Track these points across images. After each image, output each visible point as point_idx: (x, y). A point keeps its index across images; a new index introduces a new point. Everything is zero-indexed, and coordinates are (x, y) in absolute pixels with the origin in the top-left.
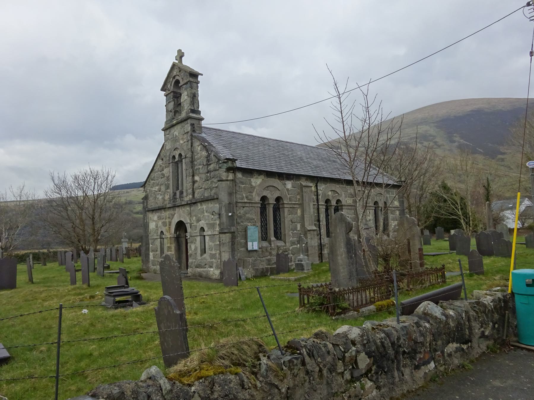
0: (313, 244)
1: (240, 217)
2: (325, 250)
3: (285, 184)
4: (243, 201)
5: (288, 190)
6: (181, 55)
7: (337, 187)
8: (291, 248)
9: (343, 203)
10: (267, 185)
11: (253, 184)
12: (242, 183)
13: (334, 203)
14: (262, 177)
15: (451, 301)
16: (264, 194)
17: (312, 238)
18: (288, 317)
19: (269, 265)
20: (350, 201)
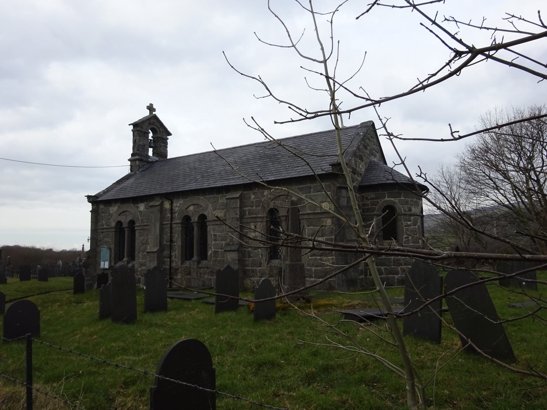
2: (179, 274)
5: (140, 212)
6: (150, 132)
7: (202, 200)
8: (139, 269)
9: (210, 217)
10: (122, 211)
11: (111, 212)
12: (103, 212)
13: (195, 219)
14: (118, 204)
15: (214, 367)
16: (120, 219)
17: (151, 261)
18: (479, 388)
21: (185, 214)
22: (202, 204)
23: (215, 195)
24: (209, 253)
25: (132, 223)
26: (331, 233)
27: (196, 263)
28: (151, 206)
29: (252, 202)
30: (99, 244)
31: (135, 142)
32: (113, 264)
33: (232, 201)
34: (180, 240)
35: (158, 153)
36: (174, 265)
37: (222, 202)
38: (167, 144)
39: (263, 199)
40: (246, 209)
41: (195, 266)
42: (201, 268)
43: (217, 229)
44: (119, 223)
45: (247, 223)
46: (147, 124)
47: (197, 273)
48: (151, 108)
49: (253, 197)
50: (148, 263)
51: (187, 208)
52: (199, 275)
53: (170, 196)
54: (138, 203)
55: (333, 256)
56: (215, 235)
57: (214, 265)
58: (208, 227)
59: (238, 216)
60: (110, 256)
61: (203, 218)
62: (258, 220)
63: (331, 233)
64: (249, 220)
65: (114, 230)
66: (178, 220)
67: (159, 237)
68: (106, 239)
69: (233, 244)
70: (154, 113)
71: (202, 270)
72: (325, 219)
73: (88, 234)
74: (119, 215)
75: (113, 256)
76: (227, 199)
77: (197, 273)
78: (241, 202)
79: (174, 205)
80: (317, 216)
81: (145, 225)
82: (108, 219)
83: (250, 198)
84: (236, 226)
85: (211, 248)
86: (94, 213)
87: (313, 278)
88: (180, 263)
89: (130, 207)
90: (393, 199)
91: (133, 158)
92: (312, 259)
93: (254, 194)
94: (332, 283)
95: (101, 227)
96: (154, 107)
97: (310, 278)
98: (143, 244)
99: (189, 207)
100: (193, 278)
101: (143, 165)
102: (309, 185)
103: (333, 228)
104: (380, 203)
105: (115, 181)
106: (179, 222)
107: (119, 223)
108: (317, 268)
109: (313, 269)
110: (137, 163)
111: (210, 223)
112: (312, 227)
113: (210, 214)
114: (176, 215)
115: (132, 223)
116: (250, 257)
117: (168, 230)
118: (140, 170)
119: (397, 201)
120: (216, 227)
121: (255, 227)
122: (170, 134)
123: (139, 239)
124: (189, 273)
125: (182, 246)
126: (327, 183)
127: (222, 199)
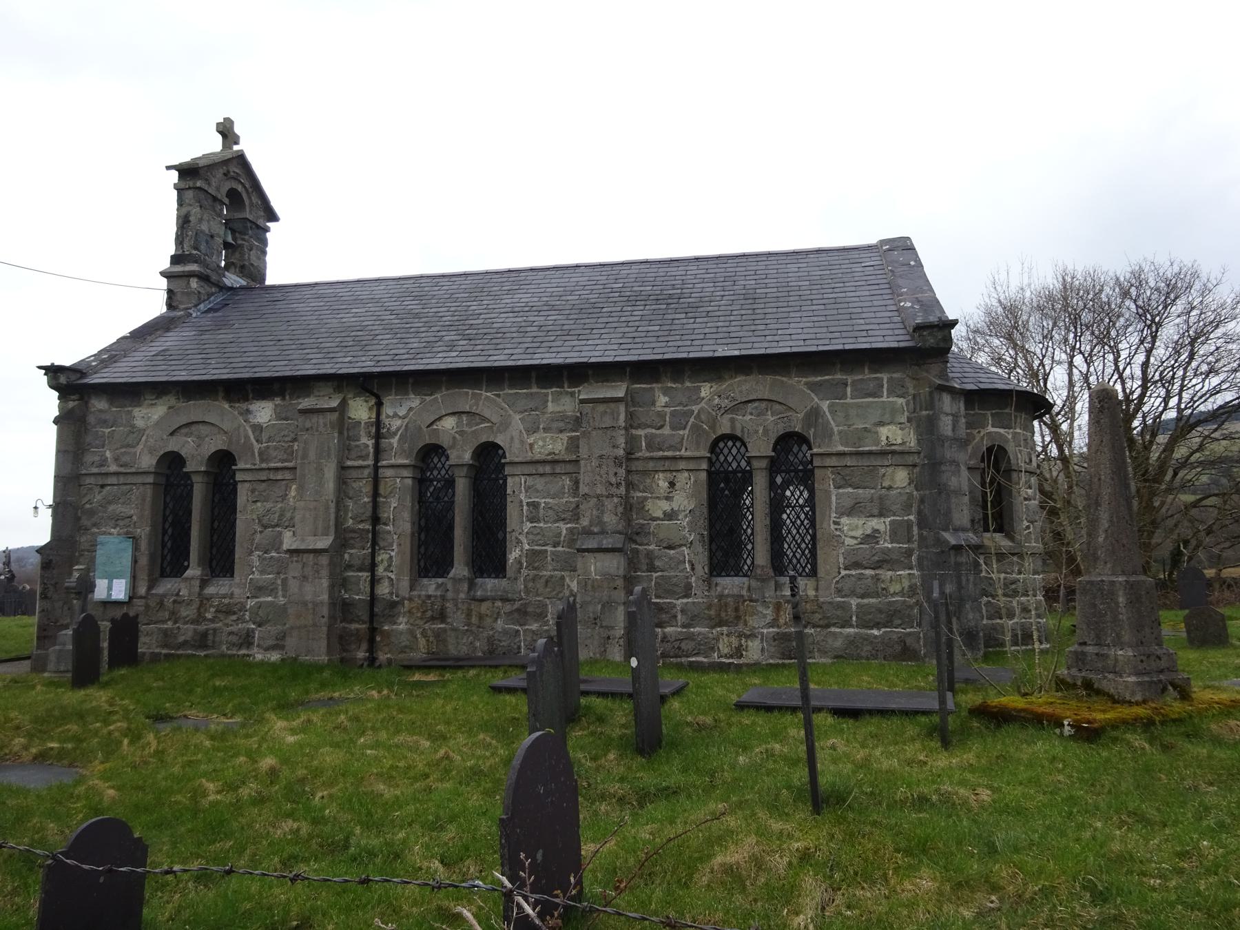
0: (309, 598)
1: (92, 513)
3: (248, 411)
4: (104, 470)
5: (258, 428)
6: (222, 201)
7: (486, 401)
8: (250, 603)
9: (513, 453)
11: (139, 423)
12: (104, 423)
14: (171, 400)
16: (173, 445)
17: (305, 578)
19: (165, 646)
20: (550, 444)
21: (428, 440)
22: (487, 413)
23: (535, 390)
24: (513, 555)
25: (223, 461)
26: (907, 508)
27: (465, 586)
28: (305, 412)
29: (661, 415)
30: (85, 522)
31: (184, 222)
32: (142, 590)
33: (601, 408)
34: (406, 515)
35: (243, 267)
36: (383, 590)
37: (558, 409)
38: (264, 243)
39: (696, 408)
40: (641, 432)
41: (462, 596)
42: (482, 600)
43: (539, 487)
44: (172, 461)
45: (645, 473)
46: (219, 173)
47: (469, 615)
48: (226, 131)
49: (662, 400)
50: (293, 585)
51: (432, 424)
52: (474, 620)
53: (374, 385)
54: (246, 399)
55: (911, 568)
56: (534, 505)
57: (527, 591)
58: (509, 480)
59: (621, 452)
60: (135, 561)
61: (489, 454)
62: (682, 465)
63: (907, 508)
64: (651, 465)
65: (150, 479)
66: (398, 455)
67: (333, 506)
68: (117, 508)
69: (603, 532)
70: (236, 148)
71: (484, 607)
72: (890, 470)
73: (45, 490)
74: (172, 434)
75: (144, 561)
76: (582, 401)
77: (469, 615)
78: (630, 416)
79: (388, 410)
80: (866, 462)
81: (277, 469)
82: (128, 446)
83: (653, 403)
84: (613, 480)
85: (519, 542)
86: (73, 426)
87: (851, 626)
88: (405, 583)
89: (220, 412)
90: (1002, 431)
91: (179, 269)
92: (849, 576)
93: (666, 392)
94: (909, 641)
95: (95, 470)
96: (237, 130)
97: (843, 627)
98: (265, 527)
99: (440, 419)
100: (455, 630)
101: (210, 295)
102: (839, 376)
103: (910, 495)
104: (977, 439)
105: (125, 331)
106: (406, 462)
107: (172, 461)
108: (866, 601)
109: (854, 602)
110: (194, 283)
111: (518, 470)
112: (850, 490)
113: (517, 444)
114: (395, 441)
115: (223, 461)
116: (652, 568)
117: (363, 487)
118: (202, 306)
119: (1010, 437)
120: (539, 483)
121: (672, 484)
122: (273, 217)
123: (249, 510)
124: (442, 616)
125: (413, 534)
126: (895, 375)
127: (560, 403)
